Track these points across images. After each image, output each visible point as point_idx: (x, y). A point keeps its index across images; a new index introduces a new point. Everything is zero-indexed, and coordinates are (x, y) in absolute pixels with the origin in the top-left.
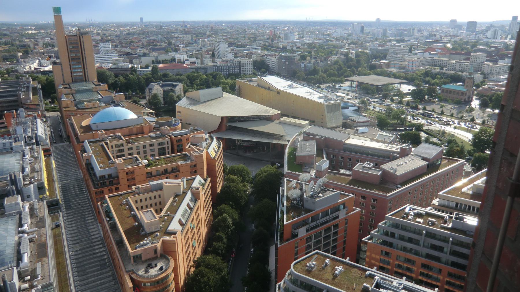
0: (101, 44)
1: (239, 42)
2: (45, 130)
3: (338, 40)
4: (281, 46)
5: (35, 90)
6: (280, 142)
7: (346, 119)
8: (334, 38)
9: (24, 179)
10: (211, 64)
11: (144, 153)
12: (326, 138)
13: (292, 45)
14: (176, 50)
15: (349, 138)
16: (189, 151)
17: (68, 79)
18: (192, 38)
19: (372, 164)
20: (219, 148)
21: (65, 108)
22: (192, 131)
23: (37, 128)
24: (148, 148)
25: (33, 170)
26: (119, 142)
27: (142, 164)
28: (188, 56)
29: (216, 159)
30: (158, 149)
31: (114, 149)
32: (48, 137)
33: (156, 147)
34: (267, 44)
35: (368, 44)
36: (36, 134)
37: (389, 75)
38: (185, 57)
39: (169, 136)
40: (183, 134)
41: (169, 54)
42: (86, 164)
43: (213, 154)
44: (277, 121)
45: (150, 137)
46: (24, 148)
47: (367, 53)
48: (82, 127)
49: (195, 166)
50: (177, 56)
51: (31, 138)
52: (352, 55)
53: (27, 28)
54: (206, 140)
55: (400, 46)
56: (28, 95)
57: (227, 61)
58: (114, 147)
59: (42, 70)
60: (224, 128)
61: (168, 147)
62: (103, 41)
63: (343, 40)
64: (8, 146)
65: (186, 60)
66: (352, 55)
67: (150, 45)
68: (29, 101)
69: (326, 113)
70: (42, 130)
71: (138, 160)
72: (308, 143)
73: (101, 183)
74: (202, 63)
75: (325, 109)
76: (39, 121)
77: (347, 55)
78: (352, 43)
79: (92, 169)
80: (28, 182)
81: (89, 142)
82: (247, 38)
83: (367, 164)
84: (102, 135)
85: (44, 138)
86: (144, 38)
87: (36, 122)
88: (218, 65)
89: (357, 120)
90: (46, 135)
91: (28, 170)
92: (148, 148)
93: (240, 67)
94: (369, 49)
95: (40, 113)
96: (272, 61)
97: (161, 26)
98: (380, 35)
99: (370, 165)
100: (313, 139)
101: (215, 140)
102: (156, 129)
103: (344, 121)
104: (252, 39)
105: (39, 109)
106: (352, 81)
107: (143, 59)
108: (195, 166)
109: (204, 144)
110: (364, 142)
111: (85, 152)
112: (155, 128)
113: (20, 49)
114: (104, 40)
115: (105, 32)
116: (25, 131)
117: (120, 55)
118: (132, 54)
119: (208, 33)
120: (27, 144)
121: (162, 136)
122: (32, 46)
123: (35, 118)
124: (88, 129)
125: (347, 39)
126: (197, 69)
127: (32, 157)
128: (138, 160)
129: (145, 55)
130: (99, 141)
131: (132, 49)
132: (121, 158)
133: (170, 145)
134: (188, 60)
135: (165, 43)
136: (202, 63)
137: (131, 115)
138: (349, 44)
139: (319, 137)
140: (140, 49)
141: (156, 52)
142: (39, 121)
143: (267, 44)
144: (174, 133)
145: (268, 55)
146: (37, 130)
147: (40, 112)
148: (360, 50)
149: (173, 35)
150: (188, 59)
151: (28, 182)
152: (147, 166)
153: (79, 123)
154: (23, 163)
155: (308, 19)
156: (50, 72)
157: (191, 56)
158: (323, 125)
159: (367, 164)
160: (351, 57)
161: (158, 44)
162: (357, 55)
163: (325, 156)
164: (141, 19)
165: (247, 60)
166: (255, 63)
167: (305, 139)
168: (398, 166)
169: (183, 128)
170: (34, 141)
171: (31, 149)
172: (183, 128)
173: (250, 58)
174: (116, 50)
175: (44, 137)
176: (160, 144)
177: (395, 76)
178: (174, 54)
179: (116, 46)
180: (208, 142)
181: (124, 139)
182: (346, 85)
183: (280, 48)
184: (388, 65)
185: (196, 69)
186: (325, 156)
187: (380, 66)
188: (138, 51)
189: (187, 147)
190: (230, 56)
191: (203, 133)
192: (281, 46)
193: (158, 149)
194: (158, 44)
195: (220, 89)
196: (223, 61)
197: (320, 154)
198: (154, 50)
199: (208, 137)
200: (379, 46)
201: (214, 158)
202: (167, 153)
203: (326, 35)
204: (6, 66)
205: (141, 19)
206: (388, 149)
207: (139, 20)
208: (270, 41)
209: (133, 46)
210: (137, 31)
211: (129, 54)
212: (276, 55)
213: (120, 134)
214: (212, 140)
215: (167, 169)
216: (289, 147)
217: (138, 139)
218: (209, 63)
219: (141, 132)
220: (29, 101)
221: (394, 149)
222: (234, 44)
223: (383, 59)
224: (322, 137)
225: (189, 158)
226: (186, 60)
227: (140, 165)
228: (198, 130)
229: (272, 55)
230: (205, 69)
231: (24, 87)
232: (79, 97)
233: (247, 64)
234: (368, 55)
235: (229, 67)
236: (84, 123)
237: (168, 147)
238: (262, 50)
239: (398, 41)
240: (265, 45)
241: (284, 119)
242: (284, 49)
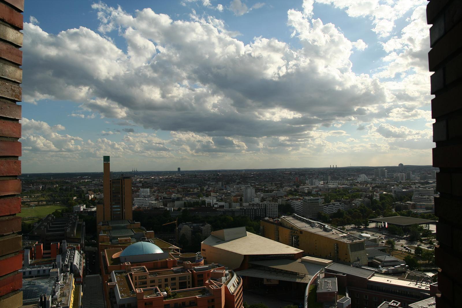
0: (141, 190)
1: (266, 188)
2: (80, 260)
3: (362, 184)
4: (306, 191)
5: (79, 227)
6: (302, 281)
7: (372, 258)
8: (358, 182)
9: (52, 303)
10: (238, 207)
11: (165, 281)
12: (348, 275)
13: (317, 190)
14: (207, 196)
15: (373, 275)
16: (207, 285)
18: (222, 185)
19: (399, 303)
20: (238, 283)
21: (101, 242)
22: (213, 267)
23: (74, 258)
24: (170, 282)
25: (63, 295)
26: (143, 274)
27: (160, 295)
28: (217, 201)
29: (235, 294)
30: (179, 283)
31: (138, 281)
32: (82, 267)
33: (177, 281)
34: (293, 189)
35: (392, 187)
36: (72, 263)
37: (416, 215)
38: (215, 201)
39: (191, 271)
40: (207, 269)
41: (201, 198)
42: (110, 293)
43: (232, 289)
44: (299, 260)
45: (173, 270)
46: (59, 274)
47: (391, 196)
48: (112, 259)
49: (213, 300)
50: (208, 200)
51: (67, 266)
52: (377, 197)
53: (85, 177)
54: (226, 276)
55: (425, 188)
56: (72, 230)
57: (253, 205)
58: (137, 278)
59: (89, 211)
61: (189, 282)
62: (144, 187)
63: (367, 185)
64: (47, 272)
65: (215, 204)
66: (377, 197)
67: (183, 191)
68: (72, 235)
69: (350, 252)
70: (77, 259)
71: (158, 291)
72: (329, 280)
74: (230, 206)
75: (349, 247)
76: (77, 252)
77: (371, 198)
78: (376, 186)
79: (114, 297)
80: (55, 306)
81: (115, 273)
82: (274, 184)
83: (394, 302)
84: (128, 266)
85: (78, 268)
87: (74, 253)
88: (245, 208)
89: (383, 259)
90: (80, 264)
91: (58, 294)
92: (170, 282)
93: (266, 210)
94: (393, 191)
95: (79, 246)
96: (297, 203)
97: (196, 175)
98: (404, 179)
99: (397, 303)
100: (333, 276)
101: (235, 276)
102: (180, 263)
103: (370, 261)
104: (278, 185)
105: (79, 243)
107: (177, 203)
108: (213, 300)
109: (223, 278)
110: (390, 279)
111: (110, 281)
112: (179, 263)
113: (75, 194)
114: (145, 185)
115: (146, 180)
116: (63, 260)
118: (167, 199)
119: (238, 181)
120: (62, 271)
121: (184, 270)
122: (85, 192)
123: (74, 249)
124: (117, 261)
125: (371, 183)
126: (225, 212)
127: (65, 283)
128: (158, 291)
129: (178, 199)
130: (125, 272)
131: (167, 194)
132: (141, 289)
133: (191, 280)
134: (217, 204)
135: (198, 189)
136: (230, 206)
137: (159, 251)
138: (373, 188)
139: (341, 275)
140: (175, 194)
141: (188, 197)
142: (77, 252)
143: (293, 189)
144: (196, 268)
145: (292, 199)
146: (73, 260)
147: (79, 245)
148: (384, 193)
150: (217, 203)
151: (55, 306)
152: (168, 296)
153: (110, 255)
154: (55, 288)
155: (332, 166)
156: (95, 212)
157: (221, 200)
158: (346, 263)
159: (394, 302)
160: (375, 200)
161: (192, 190)
162: (382, 198)
163: (347, 294)
165: (273, 203)
166: (280, 207)
167: (326, 276)
168: (429, 305)
169: (205, 263)
170: (69, 269)
171: (65, 277)
172: (205, 263)
173: (276, 201)
174: (154, 195)
175: (78, 266)
176: (180, 278)
177: (423, 216)
179: (154, 192)
180: (228, 277)
181: (148, 272)
183: (306, 193)
184: (414, 206)
185: (223, 212)
186: (347, 294)
187: (406, 207)
189: (207, 282)
190: (257, 200)
191: (223, 269)
192: (306, 191)
193: (179, 283)
194: (192, 190)
195: (244, 228)
196: (250, 205)
197: (341, 292)
198: (187, 195)
199: (228, 273)
200: (404, 188)
201: (233, 293)
202: (188, 287)
203: (350, 180)
206: (416, 287)
207: (177, 170)
208: (295, 187)
209: (169, 191)
210: (174, 179)
212: (300, 199)
213: (144, 267)
214: (232, 276)
215: (185, 302)
216: (310, 285)
217: (160, 272)
218: (237, 207)
219: (165, 265)
220: (72, 235)
221: (423, 288)
222: (261, 189)
223: (408, 200)
224: (344, 274)
225: (208, 292)
226: (215, 204)
227: (159, 296)
228: (219, 267)
229: (297, 199)
230: (233, 212)
231: (71, 224)
233: (273, 207)
234: (393, 198)
235: (255, 210)
236: (115, 256)
237: (189, 282)
239: (422, 184)
240: (291, 190)
241: (307, 258)
242: (309, 194)
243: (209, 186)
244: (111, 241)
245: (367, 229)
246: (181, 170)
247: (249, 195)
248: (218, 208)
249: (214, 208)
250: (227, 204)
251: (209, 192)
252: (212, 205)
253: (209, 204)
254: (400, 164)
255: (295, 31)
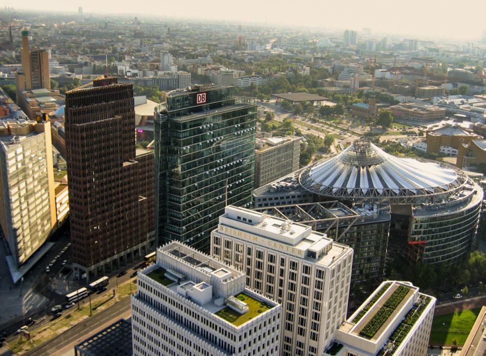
17: (29, 86)
38: (128, 69)
60: (143, 123)
73: (199, 217)
74: (144, 75)
86: (84, 41)
106: (278, 97)
117: (61, 63)
134: (130, 71)
136: (144, 75)
149: (120, 37)
150: (131, 70)
157: (136, 67)
164: (80, 9)
178: (117, 63)
182: (273, 101)
188: (79, 60)
194: (102, 50)
204: (1, 38)
205: (80, 9)
207: (77, 10)
211: (69, 62)
230: (145, 81)
232: (40, 100)
237: (453, 151)
238: (131, 67)
243: (123, 45)
244: (39, 105)
245: (267, 105)
246: (84, 11)
247: (166, 63)
248: (131, 76)
249: (126, 77)
250: (141, 72)
251: (123, 54)
252: (124, 73)
253: (122, 71)
254: (334, 355)
255: (154, 253)
